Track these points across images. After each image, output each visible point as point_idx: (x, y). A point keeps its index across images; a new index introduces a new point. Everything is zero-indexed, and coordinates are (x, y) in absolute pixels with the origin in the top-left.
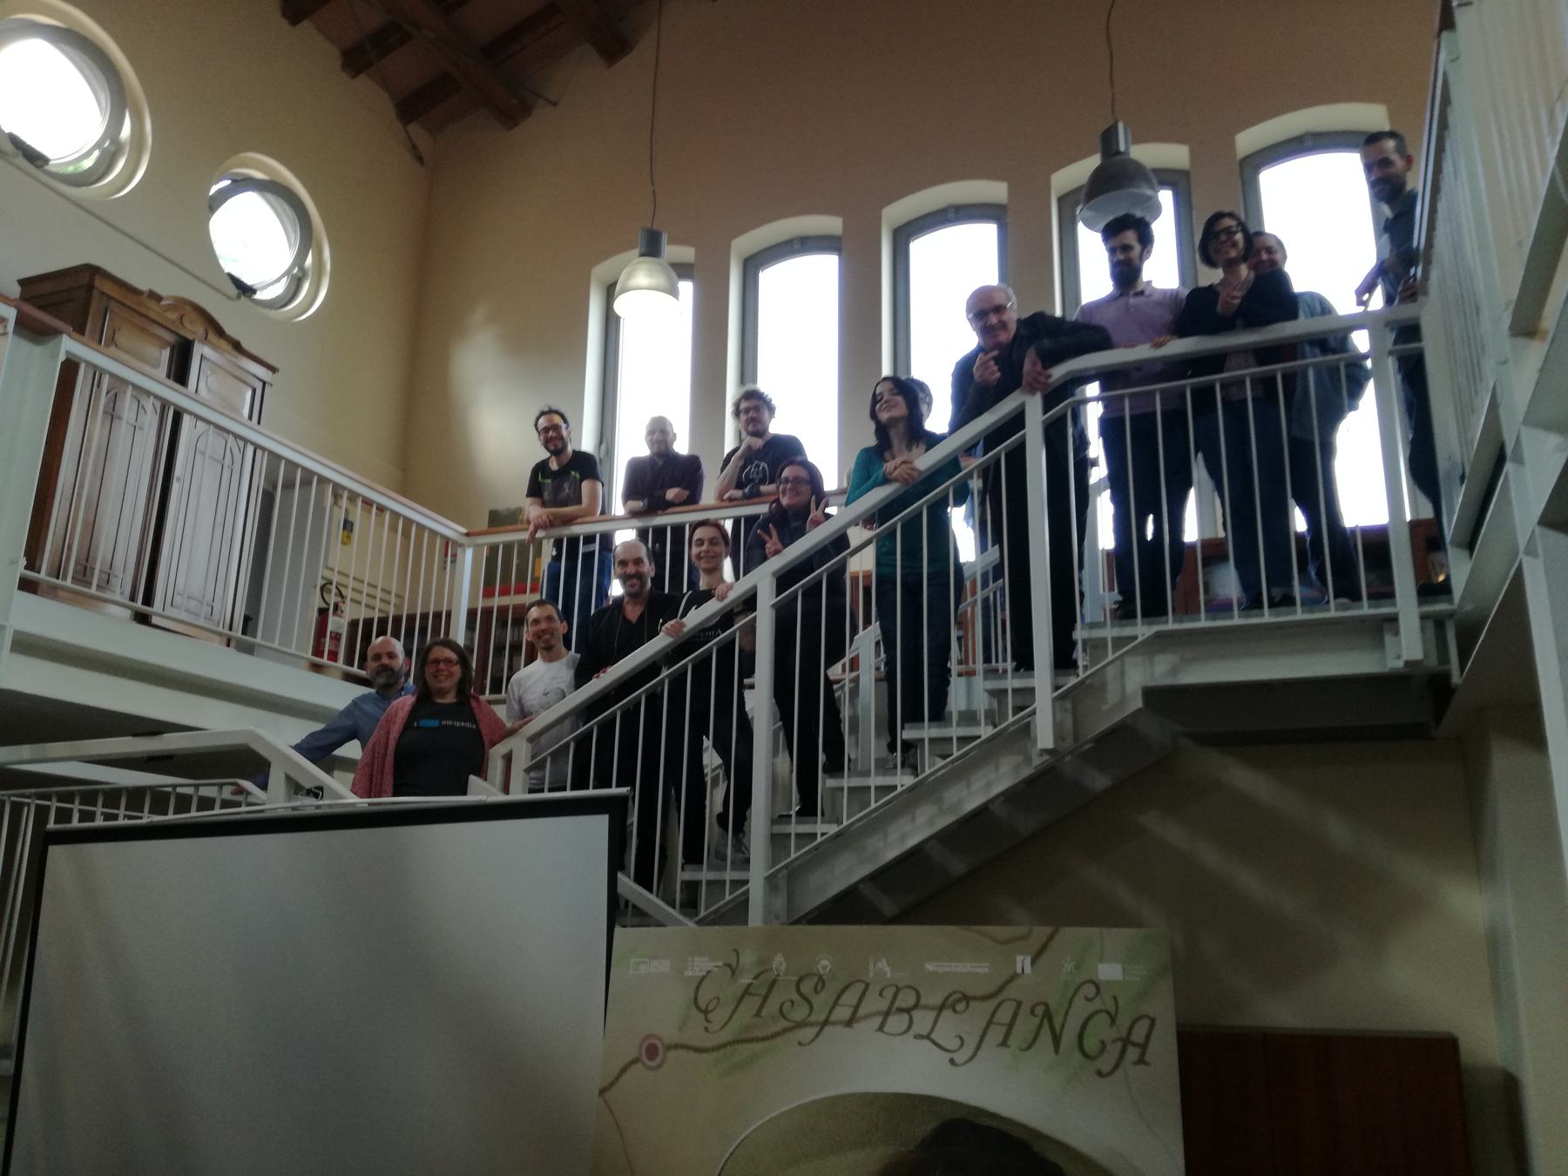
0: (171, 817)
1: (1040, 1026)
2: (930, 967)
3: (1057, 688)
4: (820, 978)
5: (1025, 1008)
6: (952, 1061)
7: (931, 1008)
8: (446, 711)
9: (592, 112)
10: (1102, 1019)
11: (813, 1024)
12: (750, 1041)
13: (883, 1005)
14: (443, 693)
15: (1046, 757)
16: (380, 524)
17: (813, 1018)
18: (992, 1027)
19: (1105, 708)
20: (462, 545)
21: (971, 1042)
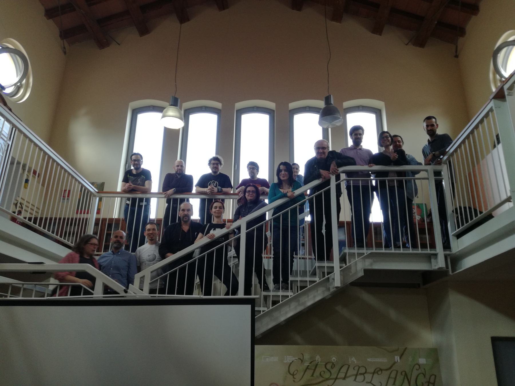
0: (69, 297)
1: (404, 378)
2: (369, 360)
3: (341, 267)
4: (333, 363)
5: (399, 374)
7: (371, 373)
9: (130, 51)
10: (421, 377)
11: (332, 379)
13: (355, 372)
15: (335, 289)
17: (331, 377)
19: (351, 274)
20: (95, 196)
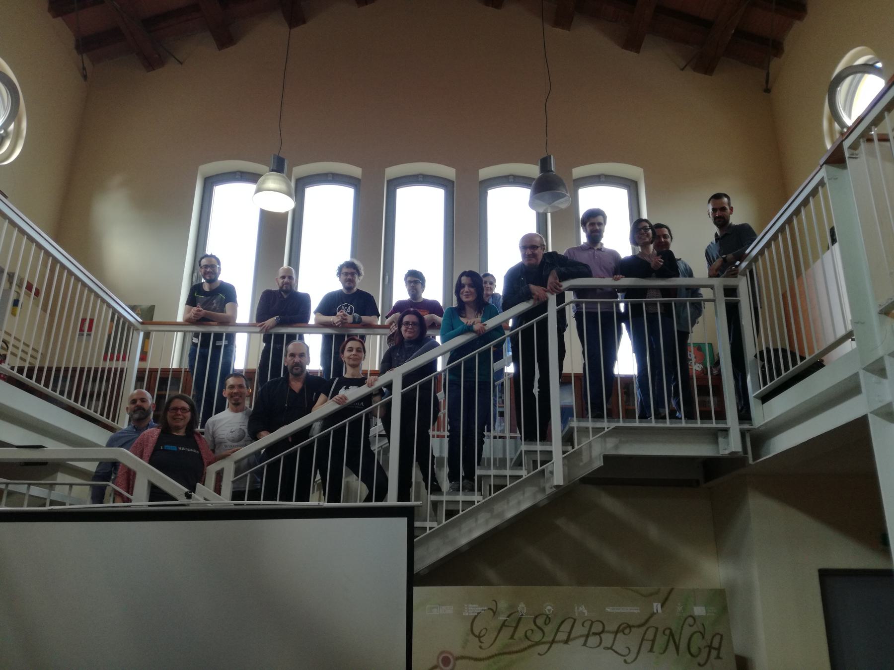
2: (608, 610)
3: (564, 453)
4: (547, 616)
5: (661, 630)
6: (625, 661)
8: (178, 441)
10: (697, 637)
12: (510, 653)
14: (178, 428)
15: (554, 489)
16: (36, 304)
17: (545, 639)
18: (645, 642)
19: (581, 464)
20: (138, 330)
21: (634, 650)
